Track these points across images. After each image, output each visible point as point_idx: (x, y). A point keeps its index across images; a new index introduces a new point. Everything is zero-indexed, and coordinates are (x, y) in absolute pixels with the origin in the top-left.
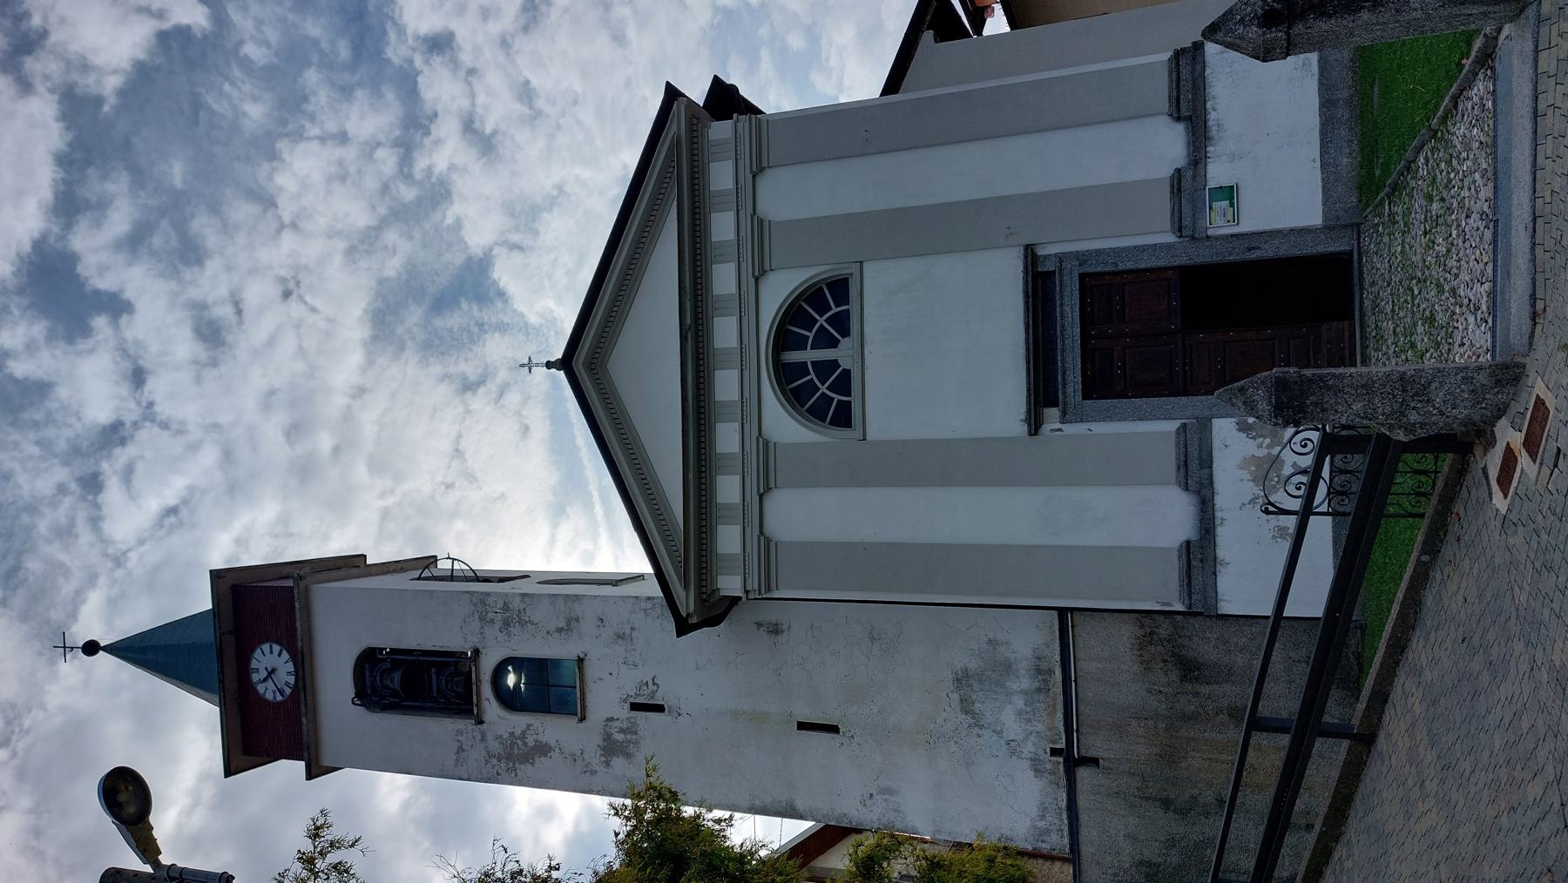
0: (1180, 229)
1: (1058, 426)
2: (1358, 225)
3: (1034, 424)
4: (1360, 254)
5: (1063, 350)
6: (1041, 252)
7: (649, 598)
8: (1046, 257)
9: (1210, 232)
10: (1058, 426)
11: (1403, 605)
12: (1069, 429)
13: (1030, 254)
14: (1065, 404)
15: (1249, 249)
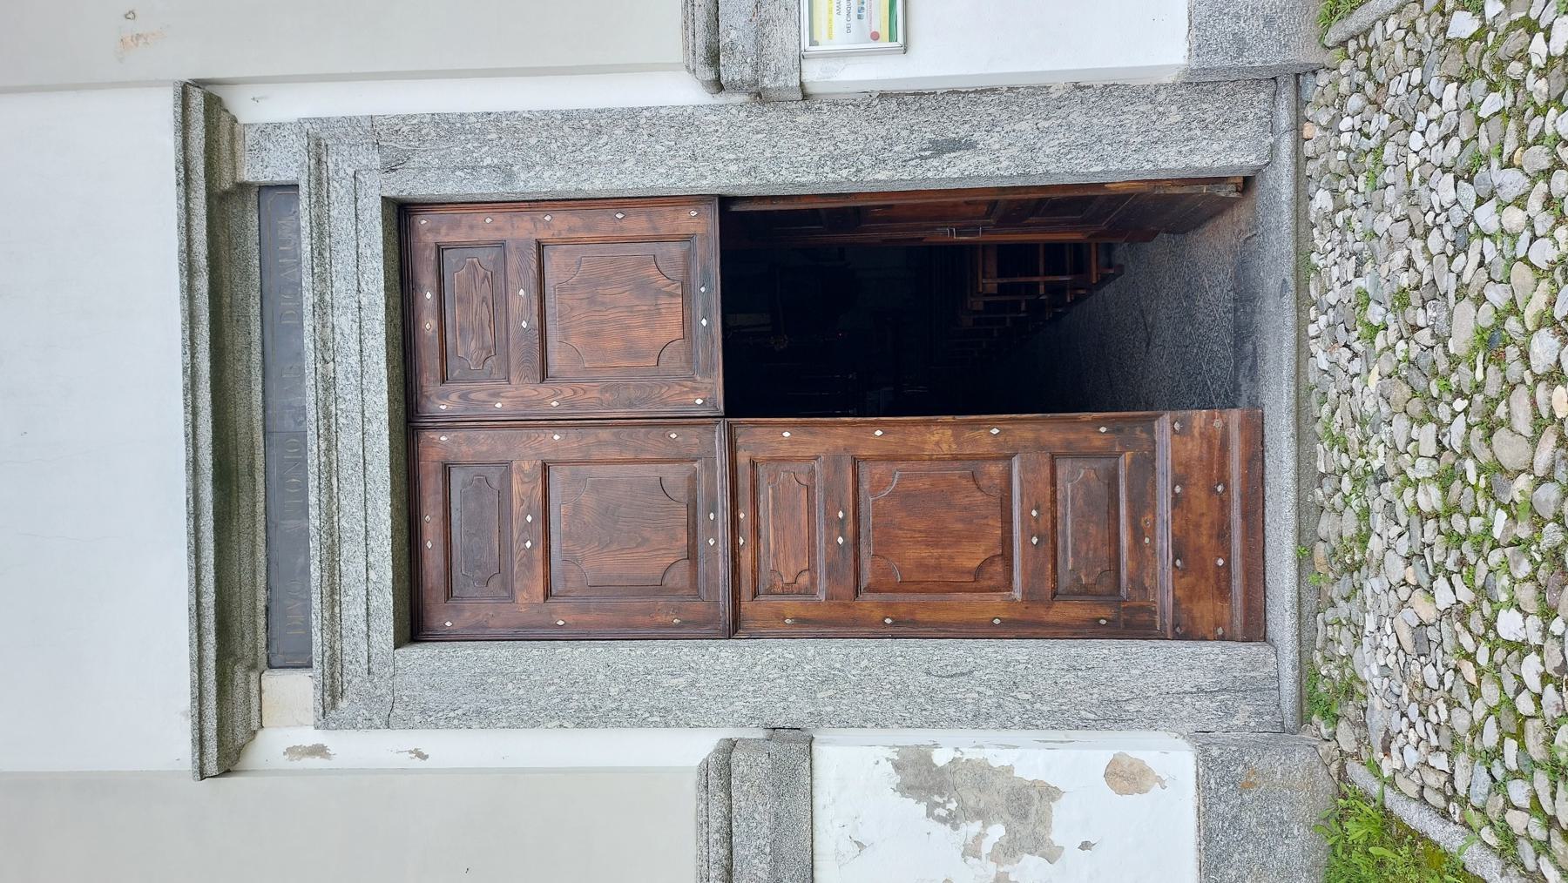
0: (713, 58)
1: (310, 736)
2: (1299, 76)
3: (225, 746)
4: (1301, 180)
5: (330, 470)
6: (250, 109)
7: (1010, 89)
8: (271, 130)
9: (814, 74)
10: (311, 737)
11: (1244, 556)
12: (359, 748)
13: (206, 111)
14: (334, 660)
15: (941, 148)
